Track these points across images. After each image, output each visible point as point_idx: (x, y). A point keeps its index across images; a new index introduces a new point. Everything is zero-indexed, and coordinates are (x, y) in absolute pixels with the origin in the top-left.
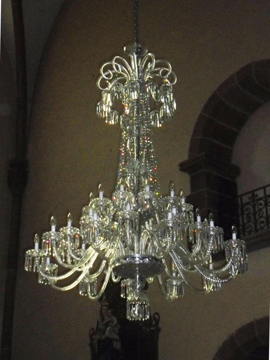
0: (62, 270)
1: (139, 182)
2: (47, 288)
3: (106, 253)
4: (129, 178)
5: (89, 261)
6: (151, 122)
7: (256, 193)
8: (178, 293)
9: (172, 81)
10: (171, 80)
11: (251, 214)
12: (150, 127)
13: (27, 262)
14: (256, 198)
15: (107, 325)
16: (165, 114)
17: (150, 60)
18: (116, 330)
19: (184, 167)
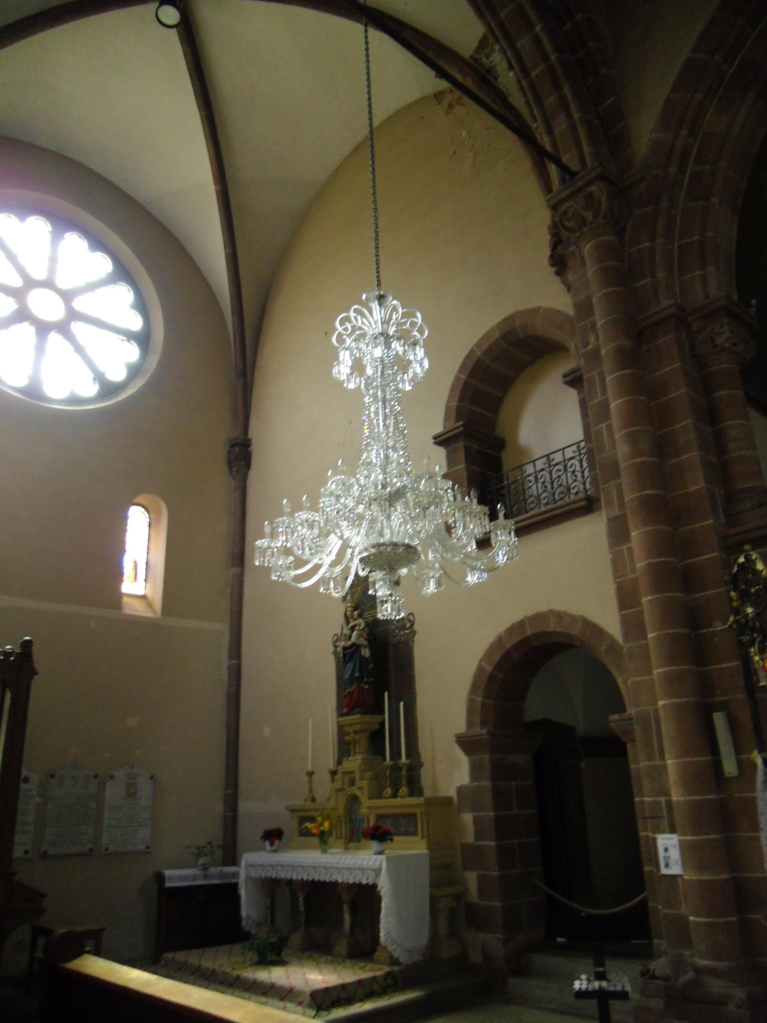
0: (300, 563)
1: (387, 457)
2: (282, 586)
3: (350, 540)
4: (374, 451)
5: (330, 552)
6: (398, 384)
7: (552, 456)
8: (437, 586)
9: (422, 333)
10: (421, 331)
11: (547, 482)
12: (398, 390)
13: (257, 555)
14: (552, 463)
15: (353, 629)
16: (415, 374)
17: (395, 309)
18: (365, 635)
19: (441, 441)
